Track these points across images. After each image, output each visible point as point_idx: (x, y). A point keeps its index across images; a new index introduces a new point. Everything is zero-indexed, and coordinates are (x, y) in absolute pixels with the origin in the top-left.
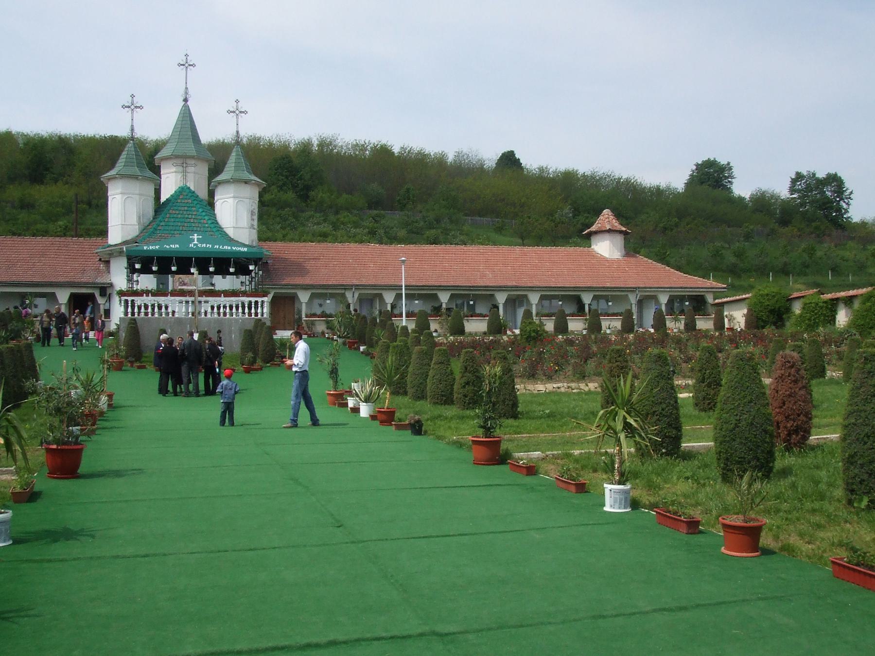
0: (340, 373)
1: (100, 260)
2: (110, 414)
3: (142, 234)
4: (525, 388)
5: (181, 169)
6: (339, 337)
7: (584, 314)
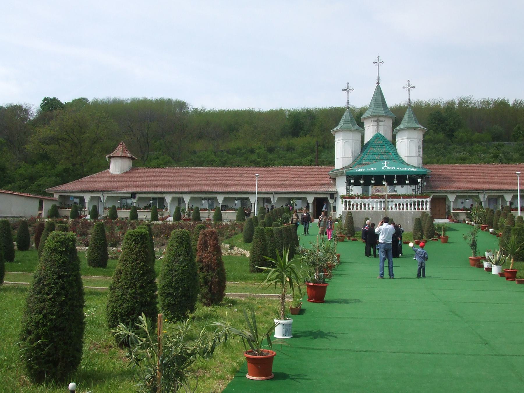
1: (331, 178)
5: (376, 123)
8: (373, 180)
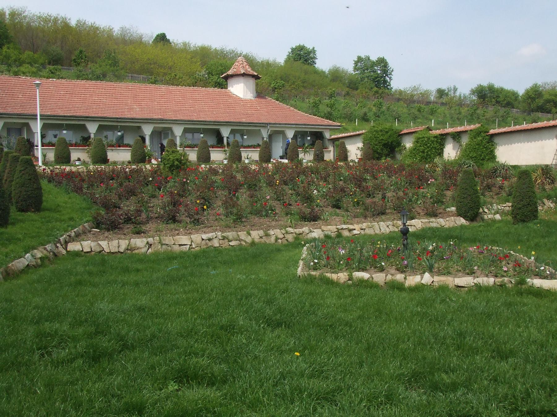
4: (160, 242)
7: (222, 146)
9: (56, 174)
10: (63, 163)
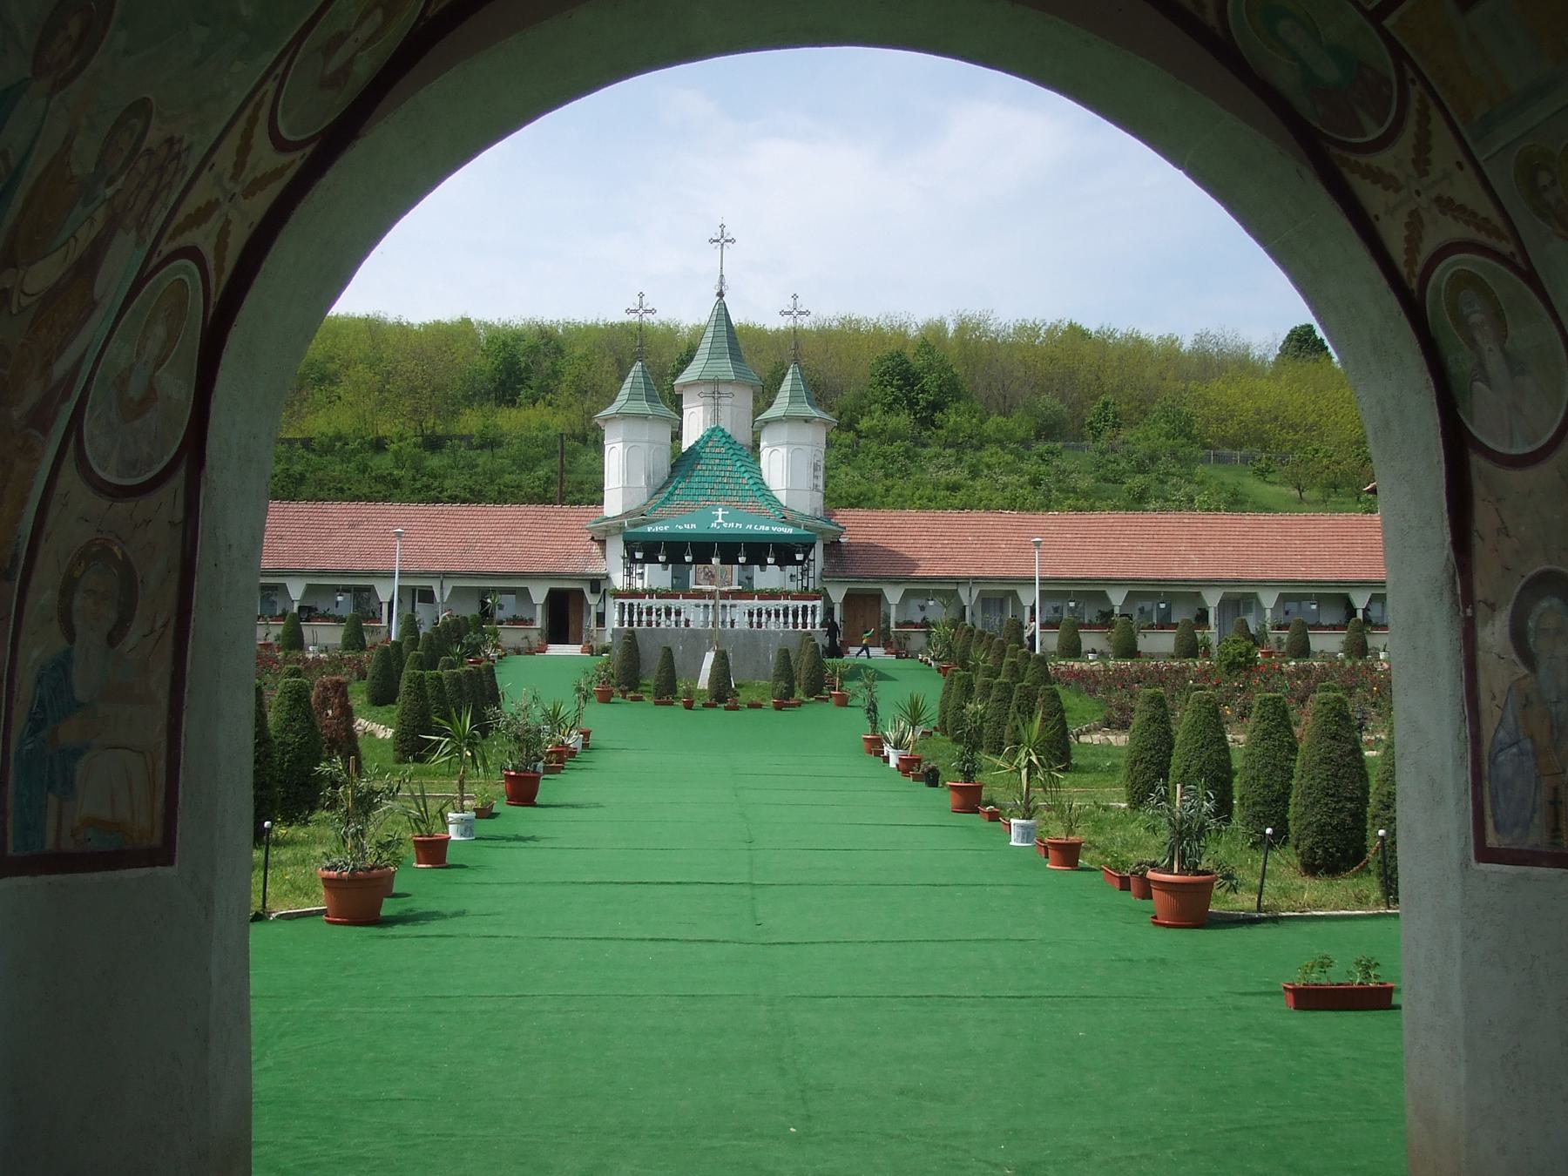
0: (879, 711)
1: (593, 539)
2: (580, 756)
3: (652, 501)
5: (710, 401)
6: (934, 659)
8: (688, 555)
9: (1062, 672)
10: (1070, 657)
